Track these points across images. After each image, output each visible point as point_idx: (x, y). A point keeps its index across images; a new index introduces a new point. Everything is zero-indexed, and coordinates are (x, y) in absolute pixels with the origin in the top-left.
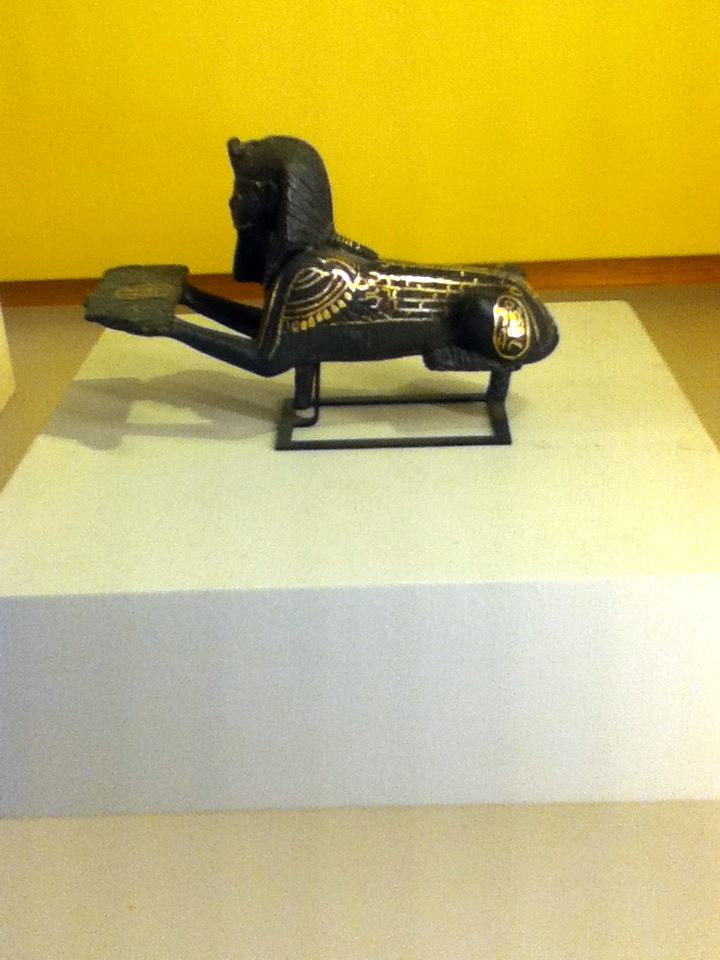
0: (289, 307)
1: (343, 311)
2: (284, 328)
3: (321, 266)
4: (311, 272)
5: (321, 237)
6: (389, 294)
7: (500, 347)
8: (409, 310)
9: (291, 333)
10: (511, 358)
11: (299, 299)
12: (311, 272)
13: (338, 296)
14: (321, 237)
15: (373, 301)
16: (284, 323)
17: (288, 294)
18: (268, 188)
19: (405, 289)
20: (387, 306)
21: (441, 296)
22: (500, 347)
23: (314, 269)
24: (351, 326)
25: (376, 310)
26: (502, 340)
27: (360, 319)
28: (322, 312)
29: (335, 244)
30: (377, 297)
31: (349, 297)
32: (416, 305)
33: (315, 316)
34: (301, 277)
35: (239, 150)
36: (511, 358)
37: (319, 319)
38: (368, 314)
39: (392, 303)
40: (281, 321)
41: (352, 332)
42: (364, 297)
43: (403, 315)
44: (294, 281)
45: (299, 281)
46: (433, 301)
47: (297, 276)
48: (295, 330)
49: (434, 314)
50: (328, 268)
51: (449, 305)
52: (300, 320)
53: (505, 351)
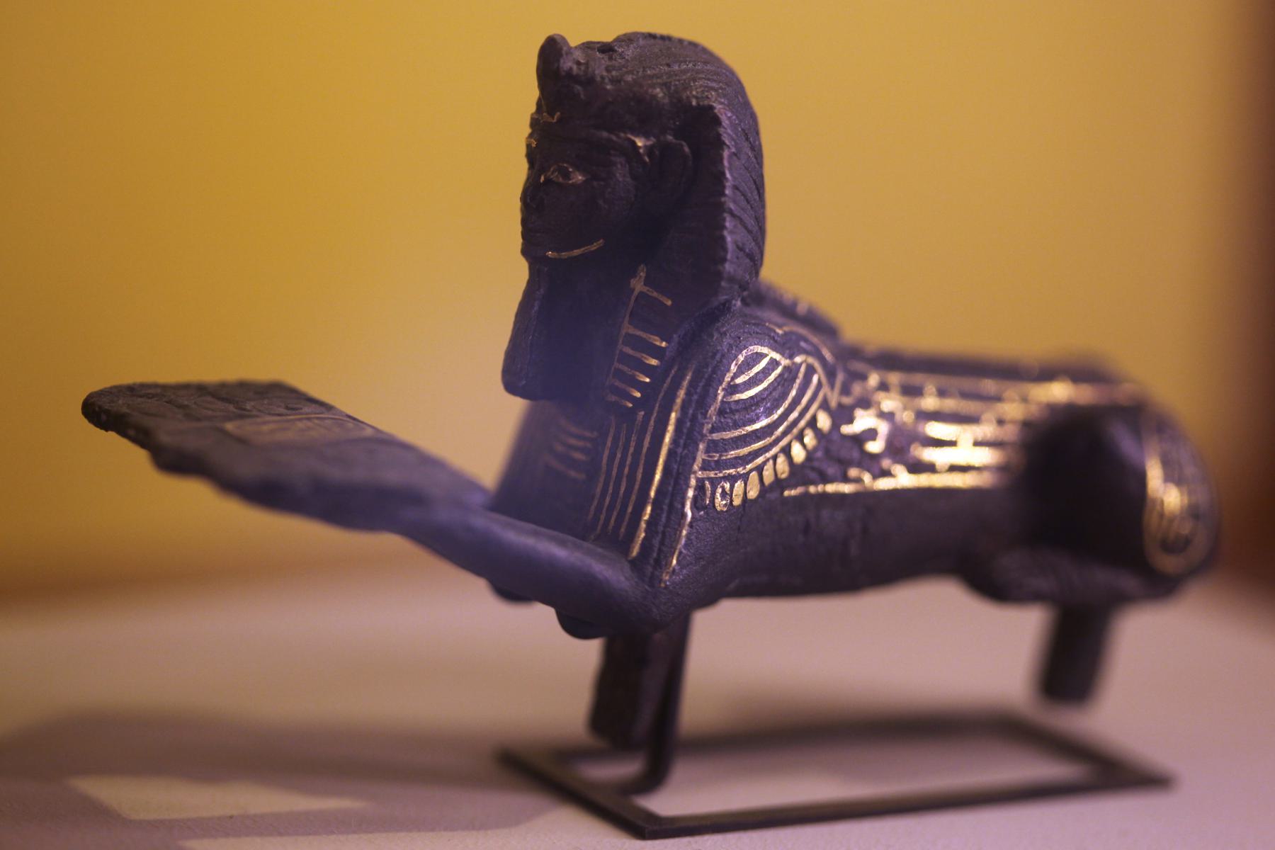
0: (713, 446)
2: (696, 504)
15: (871, 434)
16: (700, 488)
18: (661, 153)
25: (875, 457)
27: (846, 479)
28: (800, 438)
29: (760, 298)
34: (741, 371)
35: (725, 202)
38: (860, 465)
40: (693, 482)
41: (825, 513)
44: (727, 379)
45: (739, 381)
47: (733, 368)
52: (733, 479)
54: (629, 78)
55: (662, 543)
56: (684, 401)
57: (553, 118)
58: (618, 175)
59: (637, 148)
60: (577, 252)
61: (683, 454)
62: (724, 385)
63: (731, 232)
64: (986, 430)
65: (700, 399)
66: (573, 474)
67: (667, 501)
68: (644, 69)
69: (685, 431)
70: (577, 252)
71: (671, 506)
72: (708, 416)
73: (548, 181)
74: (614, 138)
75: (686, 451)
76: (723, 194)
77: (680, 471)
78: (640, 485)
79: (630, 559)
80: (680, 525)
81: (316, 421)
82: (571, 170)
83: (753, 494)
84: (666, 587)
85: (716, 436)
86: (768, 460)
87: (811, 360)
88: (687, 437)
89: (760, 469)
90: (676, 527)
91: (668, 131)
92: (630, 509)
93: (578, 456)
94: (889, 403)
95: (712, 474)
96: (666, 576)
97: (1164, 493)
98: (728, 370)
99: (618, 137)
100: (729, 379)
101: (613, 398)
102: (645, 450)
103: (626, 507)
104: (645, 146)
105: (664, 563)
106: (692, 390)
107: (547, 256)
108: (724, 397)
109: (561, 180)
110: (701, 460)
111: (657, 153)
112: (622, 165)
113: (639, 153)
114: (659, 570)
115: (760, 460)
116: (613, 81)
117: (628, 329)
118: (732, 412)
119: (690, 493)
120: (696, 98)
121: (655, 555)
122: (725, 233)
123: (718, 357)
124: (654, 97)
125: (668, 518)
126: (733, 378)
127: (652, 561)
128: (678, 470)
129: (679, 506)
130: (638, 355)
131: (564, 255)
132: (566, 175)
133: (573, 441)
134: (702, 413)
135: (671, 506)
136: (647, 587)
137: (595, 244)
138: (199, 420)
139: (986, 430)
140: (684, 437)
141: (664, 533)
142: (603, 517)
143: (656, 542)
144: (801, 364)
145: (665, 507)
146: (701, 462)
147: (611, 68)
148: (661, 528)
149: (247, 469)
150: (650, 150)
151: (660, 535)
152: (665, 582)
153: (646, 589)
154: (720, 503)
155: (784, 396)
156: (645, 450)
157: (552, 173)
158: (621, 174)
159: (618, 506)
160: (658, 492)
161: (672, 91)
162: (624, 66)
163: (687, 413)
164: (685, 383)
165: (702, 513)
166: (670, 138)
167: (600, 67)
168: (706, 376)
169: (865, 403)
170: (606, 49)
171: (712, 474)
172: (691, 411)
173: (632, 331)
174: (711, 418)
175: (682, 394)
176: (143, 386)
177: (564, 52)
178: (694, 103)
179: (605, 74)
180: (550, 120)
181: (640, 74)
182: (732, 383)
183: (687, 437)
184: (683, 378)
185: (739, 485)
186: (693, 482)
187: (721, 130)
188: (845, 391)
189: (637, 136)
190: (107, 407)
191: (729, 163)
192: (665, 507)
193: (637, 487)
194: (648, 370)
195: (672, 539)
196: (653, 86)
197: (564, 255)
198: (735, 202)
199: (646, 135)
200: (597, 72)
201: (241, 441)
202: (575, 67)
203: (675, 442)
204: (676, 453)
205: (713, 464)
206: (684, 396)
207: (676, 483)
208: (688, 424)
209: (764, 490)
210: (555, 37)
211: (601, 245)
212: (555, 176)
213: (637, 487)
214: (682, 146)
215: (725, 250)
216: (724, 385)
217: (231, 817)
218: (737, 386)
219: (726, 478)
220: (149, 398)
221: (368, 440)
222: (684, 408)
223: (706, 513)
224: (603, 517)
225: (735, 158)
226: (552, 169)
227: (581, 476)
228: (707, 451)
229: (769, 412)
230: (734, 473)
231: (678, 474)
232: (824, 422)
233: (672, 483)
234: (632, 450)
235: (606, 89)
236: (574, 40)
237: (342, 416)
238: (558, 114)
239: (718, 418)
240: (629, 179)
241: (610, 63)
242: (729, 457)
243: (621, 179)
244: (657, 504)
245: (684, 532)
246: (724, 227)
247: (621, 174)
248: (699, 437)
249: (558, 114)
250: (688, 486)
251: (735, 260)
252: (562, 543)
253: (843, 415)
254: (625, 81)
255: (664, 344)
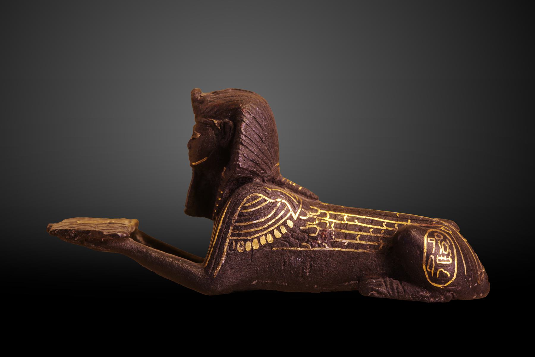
0: (236, 228)
1: (284, 236)
2: (230, 247)
3: (266, 193)
4: (258, 197)
5: (269, 173)
6: (328, 225)
7: (430, 273)
8: (346, 242)
9: (235, 250)
10: (440, 286)
11: (246, 221)
12: (258, 197)
13: (276, 226)
14: (269, 173)
15: (314, 230)
16: (231, 243)
17: (236, 216)
18: (224, 125)
19: (343, 222)
20: (325, 235)
21: (376, 231)
22: (430, 273)
23: (243, 242)
24: (291, 251)
25: (315, 239)
26: (431, 268)
27: (300, 247)
30: (316, 226)
31: (290, 224)
32: (353, 237)
33: (259, 238)
34: (248, 202)
36: (440, 286)
37: (263, 241)
38: (307, 242)
39: (331, 234)
40: (228, 240)
42: (305, 226)
43: (341, 245)
45: (247, 205)
46: (369, 234)
47: (245, 200)
48: (240, 250)
49: (371, 246)
50: (274, 195)
51: (384, 239)
52: (246, 241)
53: (435, 280)
55: (215, 262)
59: (215, 124)
65: (232, 212)
67: (218, 247)
74: (207, 120)
82: (196, 133)
85: (236, 224)
86: (262, 235)
87: (284, 201)
88: (227, 225)
98: (243, 200)
99: (208, 119)
100: (243, 204)
104: (218, 123)
108: (241, 210)
113: (216, 125)
118: (244, 216)
121: (213, 266)
127: (211, 268)
135: (219, 248)
137: (204, 159)
140: (225, 224)
144: (279, 202)
146: (231, 233)
163: (227, 216)
165: (232, 252)
166: (227, 120)
182: (244, 206)
185: (248, 244)
188: (303, 214)
199: (219, 119)
203: (222, 226)
205: (236, 235)
211: (207, 159)
218: (246, 207)
219: (241, 240)
228: (234, 229)
230: (245, 238)
233: (220, 241)
239: (238, 218)
242: (243, 232)
245: (299, 249)
251: (243, 161)
255: (222, 192)
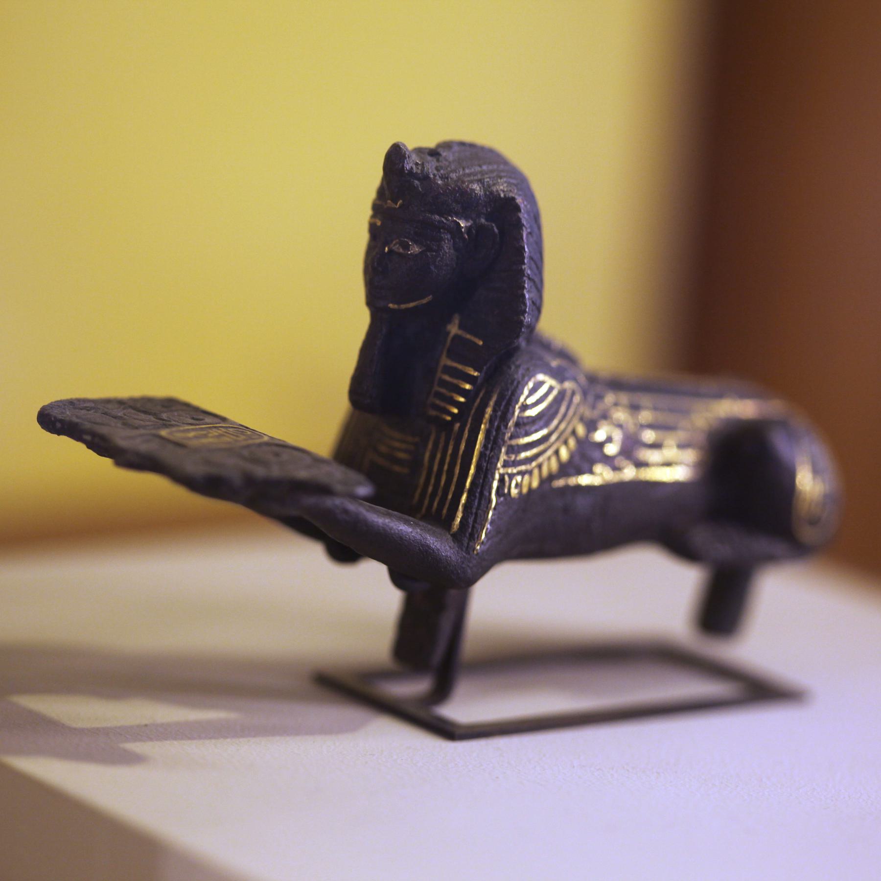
2: (499, 493)
16: (502, 480)
18: (477, 232)
28: (566, 443)
35: (525, 269)
40: (497, 476)
44: (522, 399)
54: (454, 176)
55: (475, 521)
56: (491, 416)
57: (396, 204)
58: (445, 248)
60: (412, 305)
61: (491, 456)
62: (520, 404)
63: (528, 292)
64: (682, 435)
66: (397, 468)
67: (479, 490)
68: (464, 169)
69: (492, 438)
70: (412, 305)
71: (481, 493)
72: (509, 426)
73: (390, 251)
75: (492, 453)
76: (524, 263)
77: (488, 468)
78: (458, 478)
79: (451, 533)
80: (488, 508)
81: (224, 430)
83: (535, 484)
84: (478, 554)
89: (540, 466)
90: (485, 509)
91: (482, 216)
92: (450, 497)
93: (402, 455)
94: (620, 415)
95: (510, 471)
96: (478, 546)
97: (516, 430)
99: (446, 219)
101: (433, 413)
102: (461, 452)
103: (447, 495)
105: (476, 536)
106: (497, 408)
107: (389, 308)
109: (401, 250)
110: (502, 460)
111: (474, 232)
112: (448, 240)
114: (473, 541)
115: (541, 459)
116: (442, 178)
117: (445, 361)
119: (495, 484)
120: (503, 191)
121: (470, 530)
122: (525, 292)
123: (515, 383)
124: (473, 190)
125: (479, 504)
126: (525, 400)
127: (468, 535)
128: (487, 466)
129: (487, 494)
130: (455, 381)
131: (403, 306)
132: (406, 247)
133: (397, 444)
134: (504, 426)
136: (464, 554)
138: (137, 428)
139: (682, 435)
140: (491, 443)
141: (476, 514)
142: (426, 502)
143: (471, 521)
145: (477, 495)
147: (439, 168)
148: (474, 511)
149: (194, 468)
150: (469, 229)
151: (474, 516)
152: (477, 550)
153: (464, 556)
154: (514, 492)
155: (556, 413)
156: (461, 452)
157: (395, 245)
158: (447, 247)
159: (440, 493)
160: (472, 483)
161: (485, 186)
162: (448, 166)
164: (492, 403)
166: (483, 221)
167: (431, 166)
168: (507, 397)
169: (605, 416)
170: (434, 153)
171: (510, 471)
172: (496, 424)
173: (450, 363)
174: (510, 428)
175: (489, 411)
176: (79, 400)
177: (407, 156)
178: (502, 195)
179: (435, 172)
180: (394, 206)
181: (461, 173)
183: (494, 443)
184: (489, 399)
186: (497, 476)
187: (521, 215)
189: (460, 219)
190: (60, 417)
191: (527, 240)
192: (477, 495)
193: (455, 479)
194: (464, 392)
195: (482, 518)
196: (472, 182)
197: (403, 306)
198: (530, 268)
199: (466, 219)
200: (430, 171)
201: (178, 445)
202: (414, 167)
204: (486, 454)
206: (491, 412)
207: (485, 477)
208: (494, 433)
209: (542, 482)
210: (400, 144)
212: (397, 248)
213: (455, 479)
214: (493, 227)
215: (525, 305)
216: (520, 404)
217: (146, 725)
220: (88, 410)
221: (267, 444)
222: (491, 421)
223: (505, 499)
224: (426, 502)
225: (530, 236)
226: (394, 242)
227: (405, 471)
228: (507, 453)
229: (546, 425)
231: (487, 470)
232: (581, 430)
233: (482, 476)
234: (450, 452)
235: (437, 184)
236: (410, 144)
237: (237, 425)
238: (401, 201)
240: (452, 251)
241: (438, 165)
243: (447, 251)
244: (470, 492)
246: (524, 288)
247: (447, 247)
248: (502, 443)
249: (401, 201)
250: (493, 479)
251: (531, 312)
252: (406, 522)
253: (592, 426)
254: (451, 178)
255: (476, 374)
